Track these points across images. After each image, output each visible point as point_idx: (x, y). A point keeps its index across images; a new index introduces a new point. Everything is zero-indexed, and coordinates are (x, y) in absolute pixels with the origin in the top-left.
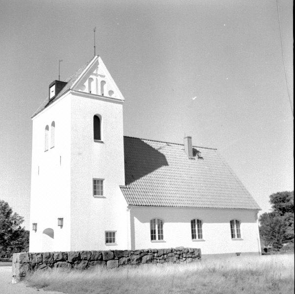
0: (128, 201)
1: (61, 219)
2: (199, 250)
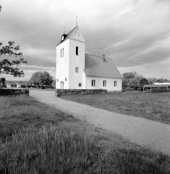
0: (86, 74)
1: (66, 79)
2: (107, 90)
